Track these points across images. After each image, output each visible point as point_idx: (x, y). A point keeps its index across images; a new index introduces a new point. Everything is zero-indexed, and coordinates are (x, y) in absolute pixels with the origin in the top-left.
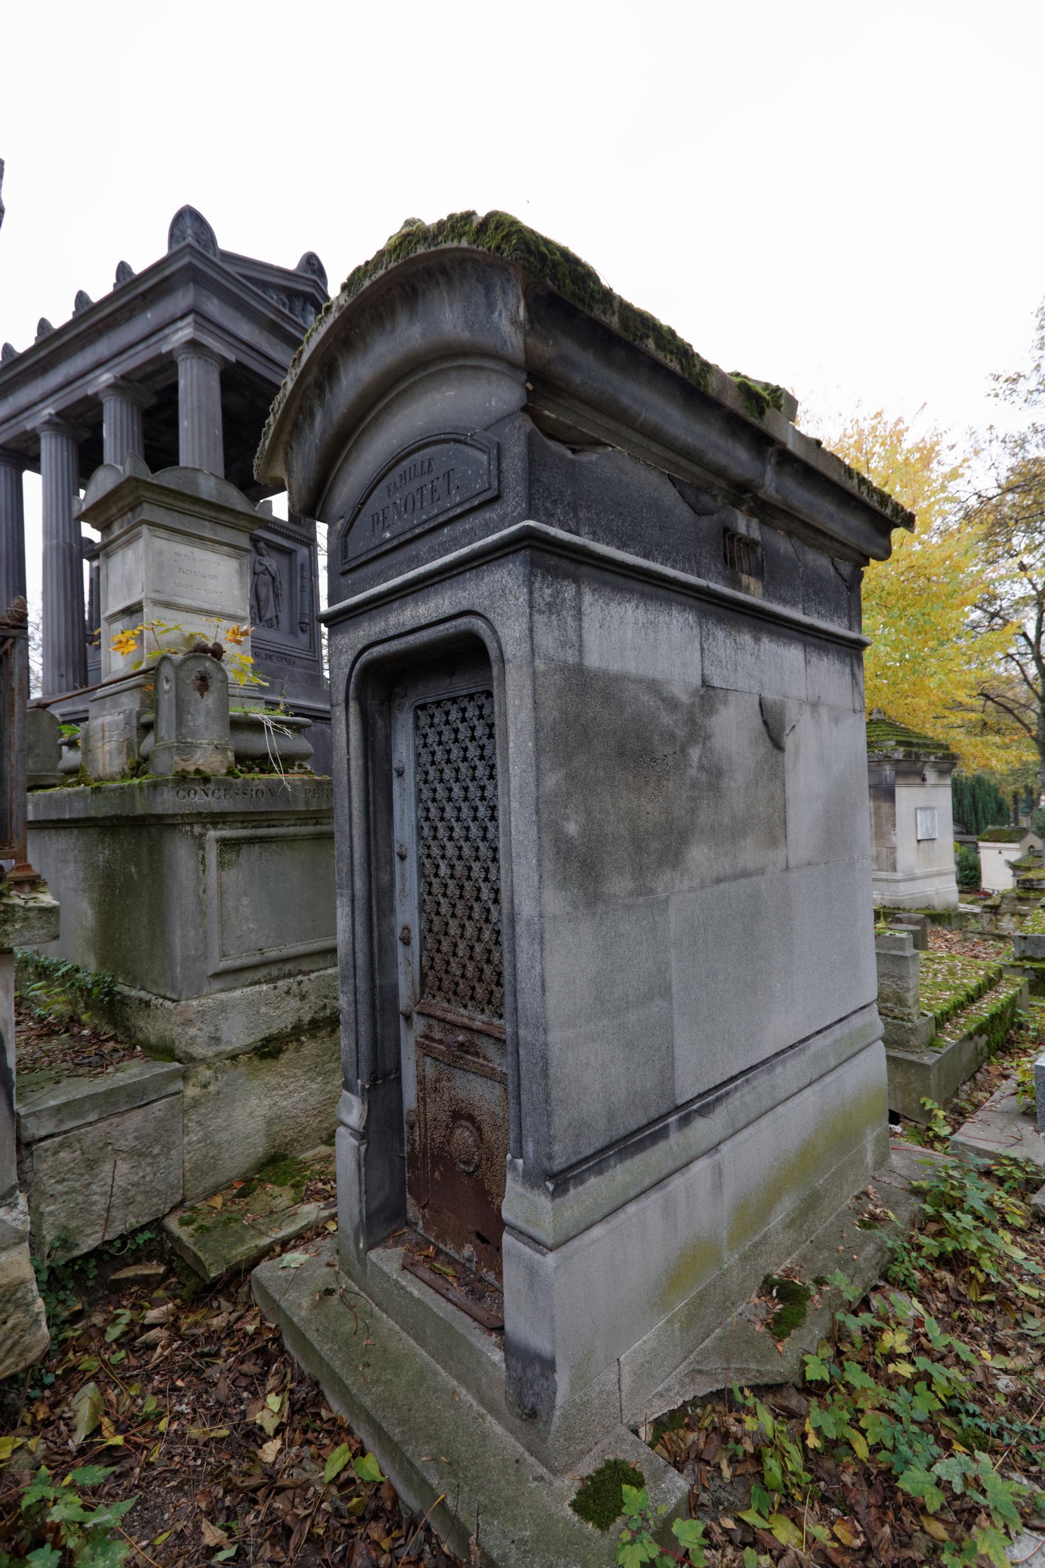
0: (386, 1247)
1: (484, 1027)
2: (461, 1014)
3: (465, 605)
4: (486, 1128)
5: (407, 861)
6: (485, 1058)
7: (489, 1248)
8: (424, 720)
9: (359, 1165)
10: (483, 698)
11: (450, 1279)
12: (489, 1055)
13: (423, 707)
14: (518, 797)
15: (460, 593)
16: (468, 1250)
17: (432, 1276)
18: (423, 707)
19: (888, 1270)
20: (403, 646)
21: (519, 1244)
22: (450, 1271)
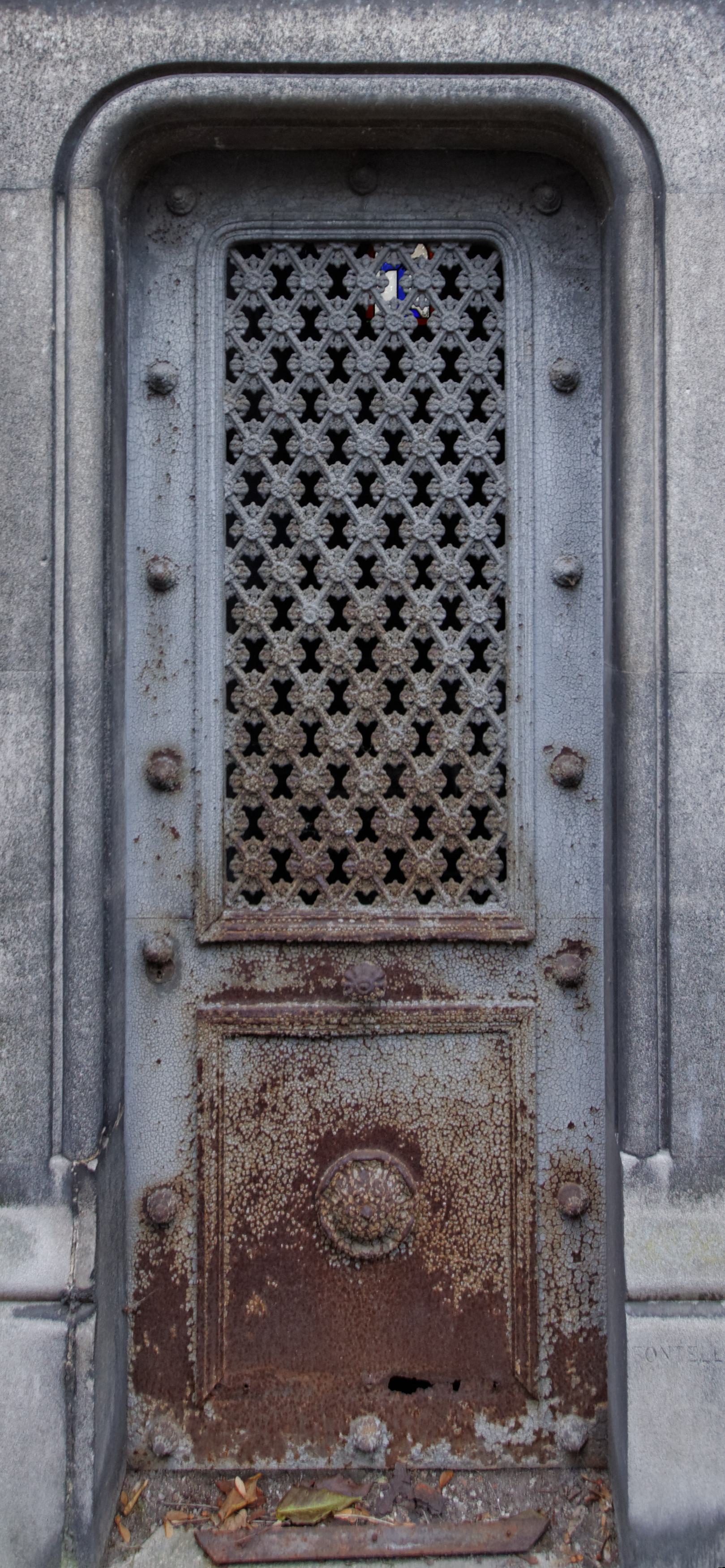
0: (124, 1555)
1: (449, 928)
2: (343, 916)
3: (552, 51)
4: (433, 1146)
5: (180, 597)
6: (435, 993)
7: (429, 1395)
8: (256, 276)
9: (69, 1383)
10: (350, 252)
11: (347, 1514)
12: (449, 984)
13: (251, 249)
14: (689, 448)
15: (537, 25)
16: (370, 1431)
17: (313, 1536)
18: (251, 249)
19: (318, 1191)
20: (182, 93)
21: (674, 1323)
22: (328, 1502)
